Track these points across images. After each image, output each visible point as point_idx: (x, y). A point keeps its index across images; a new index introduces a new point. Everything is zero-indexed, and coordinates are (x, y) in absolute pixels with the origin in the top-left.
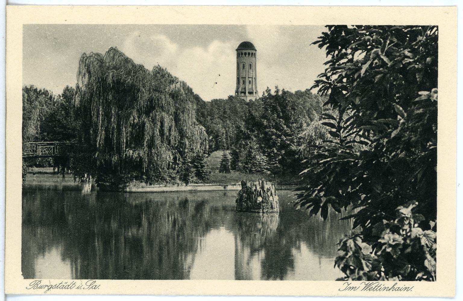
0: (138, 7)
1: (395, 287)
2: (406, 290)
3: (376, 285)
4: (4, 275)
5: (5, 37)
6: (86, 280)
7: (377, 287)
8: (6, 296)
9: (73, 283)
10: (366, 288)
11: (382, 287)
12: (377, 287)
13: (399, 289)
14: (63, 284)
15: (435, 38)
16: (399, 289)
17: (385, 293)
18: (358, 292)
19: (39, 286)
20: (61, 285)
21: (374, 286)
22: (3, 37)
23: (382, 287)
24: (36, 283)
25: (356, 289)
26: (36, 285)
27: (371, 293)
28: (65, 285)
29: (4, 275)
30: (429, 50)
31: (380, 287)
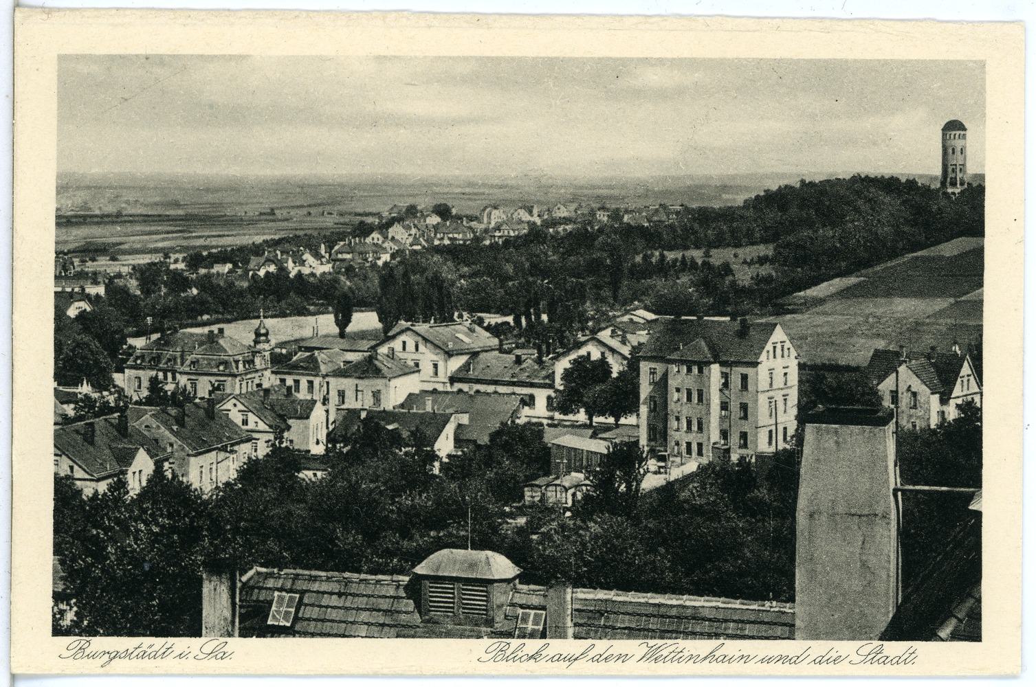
0: (480, 17)
1: (717, 654)
2: (622, 659)
3: (673, 648)
4: (10, 628)
5: (11, 96)
6: (858, 643)
7: (673, 655)
8: (14, 677)
9: (911, 651)
10: (872, 658)
11: (686, 653)
12: (673, 655)
13: (725, 659)
14: (144, 647)
15: (981, 190)
16: (889, 659)
17: (689, 668)
18: (631, 666)
19: (87, 651)
20: (880, 656)
21: (665, 653)
22: (7, 96)
23: (686, 653)
24: (80, 646)
25: (628, 657)
26: (500, 653)
27: (660, 668)
28: (149, 651)
29: (10, 628)
30: (846, 233)
31: (681, 654)
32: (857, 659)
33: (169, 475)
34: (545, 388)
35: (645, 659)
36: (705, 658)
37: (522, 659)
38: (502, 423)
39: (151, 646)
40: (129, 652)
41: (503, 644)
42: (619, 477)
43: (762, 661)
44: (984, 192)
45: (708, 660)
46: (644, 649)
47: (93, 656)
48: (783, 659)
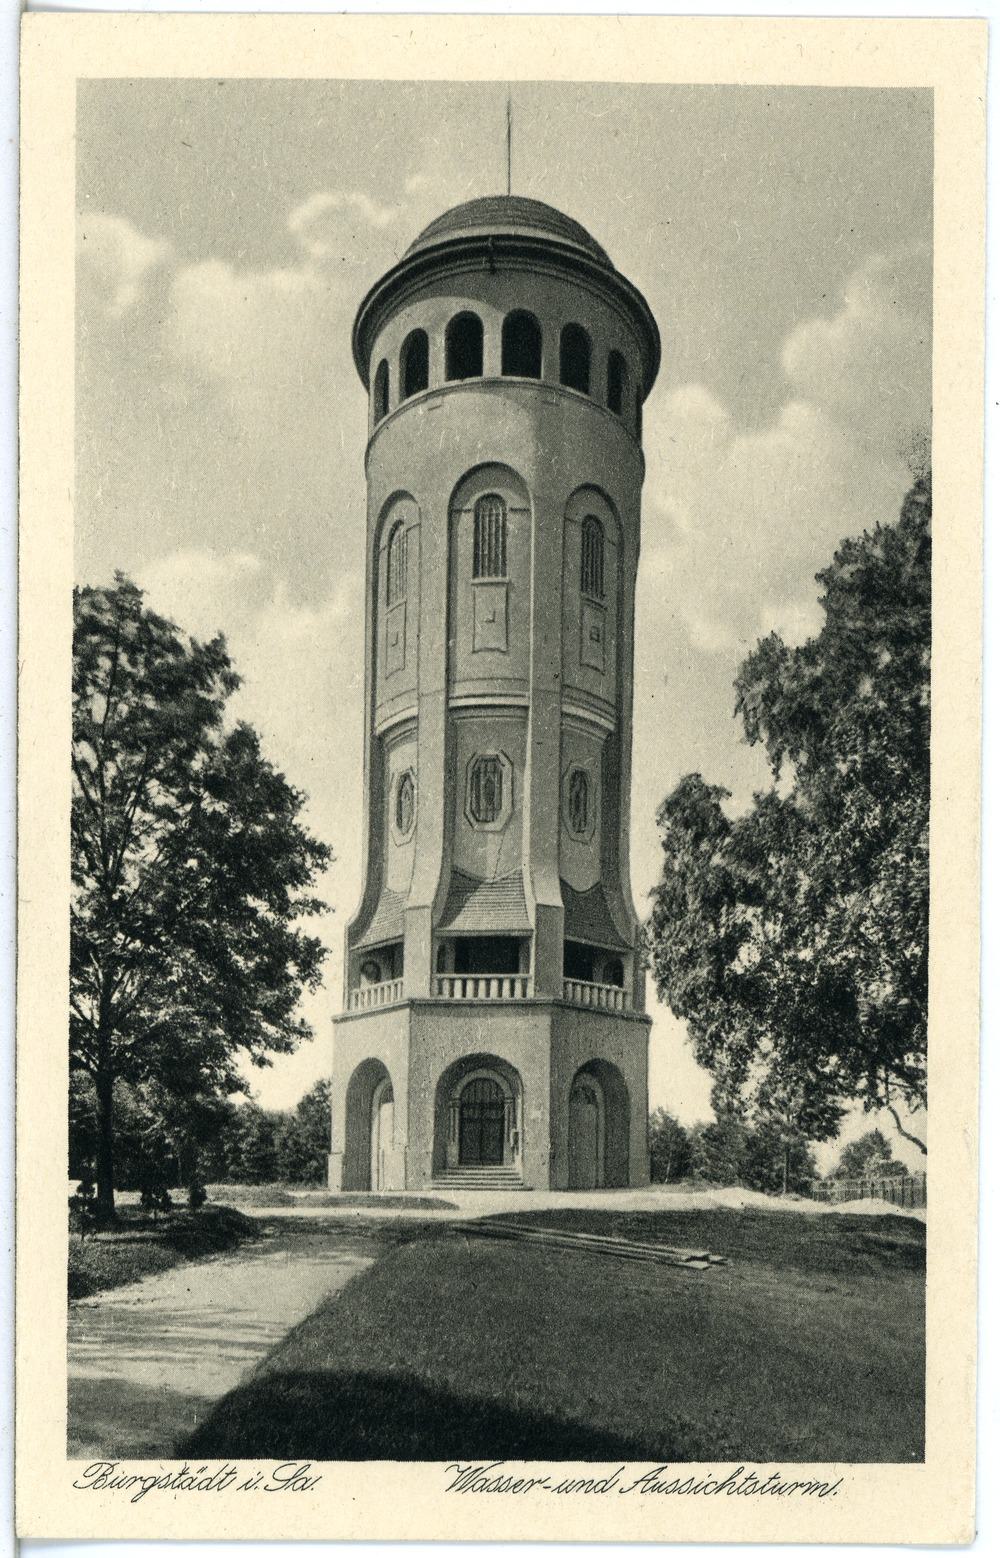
6: (276, 1463)
8: (19, 1543)
20: (184, 1477)
25: (828, 1489)
32: (274, 1485)
33: (866, 1019)
34: (372, 826)
35: (458, 1486)
36: (723, 1486)
37: (708, 1490)
38: (317, 939)
39: (202, 1470)
40: (172, 1478)
41: (105, 1467)
42: (179, 1132)
43: (558, 1489)
44: (931, 544)
45: (725, 1490)
46: (453, 1474)
47: (117, 1484)
48: (588, 1486)
